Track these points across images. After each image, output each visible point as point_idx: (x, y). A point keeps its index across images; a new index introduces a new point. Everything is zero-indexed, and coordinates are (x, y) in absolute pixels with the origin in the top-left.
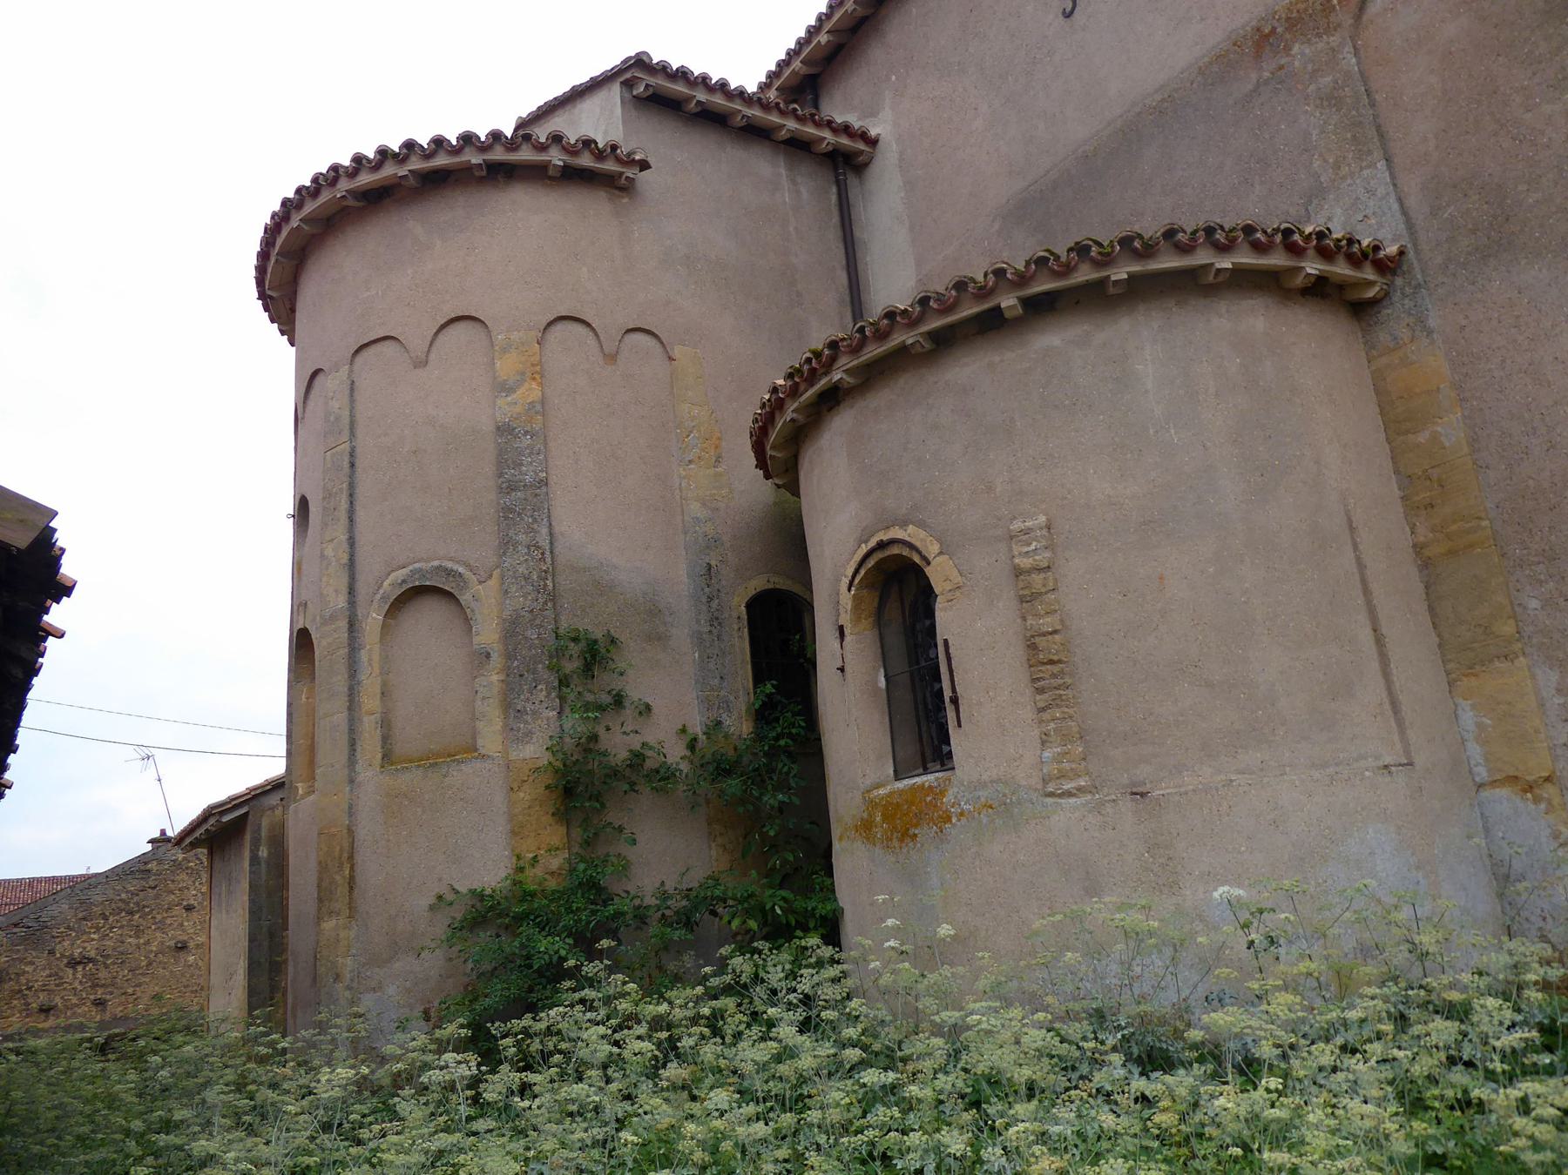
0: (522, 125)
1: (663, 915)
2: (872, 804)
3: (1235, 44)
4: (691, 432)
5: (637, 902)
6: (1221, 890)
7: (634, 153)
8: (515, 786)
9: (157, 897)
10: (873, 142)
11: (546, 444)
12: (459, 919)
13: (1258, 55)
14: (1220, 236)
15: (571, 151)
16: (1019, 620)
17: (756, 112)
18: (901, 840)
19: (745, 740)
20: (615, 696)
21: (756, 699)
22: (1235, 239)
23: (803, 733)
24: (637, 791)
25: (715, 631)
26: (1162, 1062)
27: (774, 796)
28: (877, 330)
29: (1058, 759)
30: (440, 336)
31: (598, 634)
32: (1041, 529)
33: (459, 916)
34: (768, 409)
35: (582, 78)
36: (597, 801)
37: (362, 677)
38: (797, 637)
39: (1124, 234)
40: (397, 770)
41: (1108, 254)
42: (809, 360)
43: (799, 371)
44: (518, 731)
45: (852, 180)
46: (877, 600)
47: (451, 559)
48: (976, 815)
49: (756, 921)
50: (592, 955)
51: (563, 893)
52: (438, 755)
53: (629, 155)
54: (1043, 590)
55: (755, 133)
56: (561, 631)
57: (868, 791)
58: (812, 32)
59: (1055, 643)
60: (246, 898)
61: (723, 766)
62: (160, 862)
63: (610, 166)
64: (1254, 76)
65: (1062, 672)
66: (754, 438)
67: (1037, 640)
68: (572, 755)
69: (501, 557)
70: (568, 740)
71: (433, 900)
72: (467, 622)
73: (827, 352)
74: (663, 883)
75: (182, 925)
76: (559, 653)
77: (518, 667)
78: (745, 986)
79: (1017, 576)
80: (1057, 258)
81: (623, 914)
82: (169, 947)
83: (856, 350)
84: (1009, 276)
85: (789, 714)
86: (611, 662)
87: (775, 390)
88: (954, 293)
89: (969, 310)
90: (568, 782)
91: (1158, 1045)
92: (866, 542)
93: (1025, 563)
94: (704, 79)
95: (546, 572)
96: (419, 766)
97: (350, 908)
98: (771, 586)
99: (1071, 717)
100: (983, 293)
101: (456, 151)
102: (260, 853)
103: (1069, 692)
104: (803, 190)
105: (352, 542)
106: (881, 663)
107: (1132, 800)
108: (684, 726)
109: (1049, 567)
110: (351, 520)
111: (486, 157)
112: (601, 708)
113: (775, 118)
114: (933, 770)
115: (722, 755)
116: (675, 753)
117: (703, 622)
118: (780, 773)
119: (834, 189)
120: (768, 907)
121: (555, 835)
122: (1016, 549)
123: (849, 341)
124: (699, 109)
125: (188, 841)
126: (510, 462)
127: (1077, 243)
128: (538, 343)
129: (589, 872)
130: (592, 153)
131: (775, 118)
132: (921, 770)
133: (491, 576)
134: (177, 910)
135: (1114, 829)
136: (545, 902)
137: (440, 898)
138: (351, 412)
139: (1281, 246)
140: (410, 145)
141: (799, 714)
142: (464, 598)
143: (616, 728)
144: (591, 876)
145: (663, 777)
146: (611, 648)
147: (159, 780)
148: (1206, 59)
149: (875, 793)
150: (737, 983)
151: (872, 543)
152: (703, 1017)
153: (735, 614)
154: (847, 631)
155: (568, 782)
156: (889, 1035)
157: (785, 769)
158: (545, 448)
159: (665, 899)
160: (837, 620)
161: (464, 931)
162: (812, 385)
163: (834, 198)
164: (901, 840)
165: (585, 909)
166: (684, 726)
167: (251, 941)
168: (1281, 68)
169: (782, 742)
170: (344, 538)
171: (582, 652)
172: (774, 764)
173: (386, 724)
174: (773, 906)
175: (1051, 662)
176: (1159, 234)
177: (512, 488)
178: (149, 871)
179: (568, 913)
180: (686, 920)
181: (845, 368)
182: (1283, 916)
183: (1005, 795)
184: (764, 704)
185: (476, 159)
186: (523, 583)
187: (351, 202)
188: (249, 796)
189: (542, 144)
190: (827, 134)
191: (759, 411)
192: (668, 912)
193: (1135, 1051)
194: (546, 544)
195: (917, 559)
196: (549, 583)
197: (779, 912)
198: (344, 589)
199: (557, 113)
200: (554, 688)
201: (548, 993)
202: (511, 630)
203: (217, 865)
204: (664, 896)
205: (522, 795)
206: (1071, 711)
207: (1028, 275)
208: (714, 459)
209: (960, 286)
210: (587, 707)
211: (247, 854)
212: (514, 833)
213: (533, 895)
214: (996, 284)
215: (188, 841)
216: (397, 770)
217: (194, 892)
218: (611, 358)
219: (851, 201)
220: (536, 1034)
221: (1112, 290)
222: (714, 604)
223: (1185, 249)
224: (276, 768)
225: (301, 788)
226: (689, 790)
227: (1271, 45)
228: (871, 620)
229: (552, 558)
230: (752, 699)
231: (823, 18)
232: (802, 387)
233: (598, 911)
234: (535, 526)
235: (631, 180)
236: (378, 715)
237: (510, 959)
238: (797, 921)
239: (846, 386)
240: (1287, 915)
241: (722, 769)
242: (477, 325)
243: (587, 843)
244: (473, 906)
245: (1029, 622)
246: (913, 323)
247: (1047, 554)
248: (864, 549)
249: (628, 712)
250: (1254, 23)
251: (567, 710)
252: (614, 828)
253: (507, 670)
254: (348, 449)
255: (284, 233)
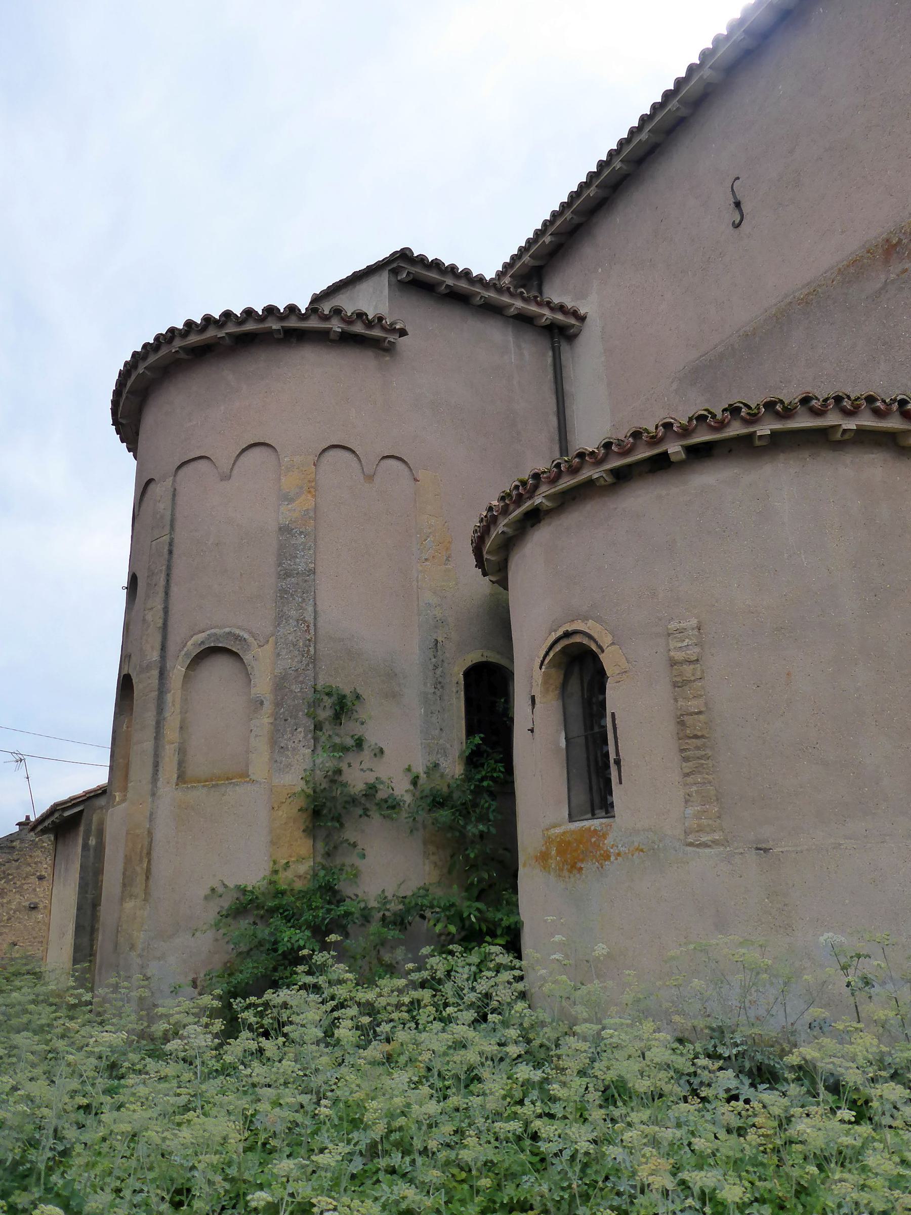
0: (317, 299)
1: (384, 915)
2: (549, 841)
3: (868, 252)
4: (428, 537)
5: (362, 905)
6: (826, 935)
7: (396, 323)
8: (276, 806)
9: (18, 868)
10: (582, 319)
11: (315, 541)
12: (226, 908)
13: (887, 261)
14: (846, 403)
15: (348, 321)
16: (672, 701)
17: (491, 294)
18: (570, 871)
19: (457, 779)
20: (357, 740)
21: (467, 747)
22: (859, 406)
23: (502, 776)
24: (368, 816)
25: (438, 693)
26: (769, 1077)
27: (476, 826)
28: (570, 466)
29: (698, 816)
30: (242, 457)
31: (347, 691)
32: (693, 629)
33: (226, 905)
34: (485, 523)
35: (345, 273)
36: (338, 821)
37: (167, 714)
38: (503, 700)
39: (769, 399)
40: (188, 788)
41: (755, 415)
42: (517, 487)
43: (509, 495)
44: (281, 763)
45: (565, 347)
46: (562, 677)
47: (238, 628)
48: (630, 856)
49: (455, 926)
50: (325, 947)
51: (306, 893)
52: (219, 778)
53: (391, 324)
54: (693, 678)
55: (491, 310)
56: (319, 687)
57: (547, 830)
58: (538, 234)
59: (700, 721)
60: (78, 875)
61: (438, 799)
62: (22, 841)
63: (377, 333)
64: (883, 277)
65: (704, 745)
66: (474, 545)
67: (686, 718)
68: (321, 784)
69: (276, 627)
70: (318, 772)
71: (208, 892)
72: (248, 676)
73: (531, 481)
74: (383, 891)
75: (34, 890)
76: (316, 703)
77: (284, 713)
78: (440, 982)
79: (672, 666)
80: (714, 416)
81: (351, 914)
82: (24, 907)
83: (553, 481)
84: (675, 428)
85: (492, 762)
86: (355, 713)
87: (490, 509)
88: (631, 440)
89: (643, 453)
90: (315, 806)
91: (766, 1062)
92: (555, 631)
93: (679, 656)
94: (453, 268)
95: (309, 640)
96: (204, 786)
97: (145, 894)
98: (484, 659)
99: (710, 782)
100: (655, 441)
101: (261, 319)
102: (90, 842)
103: (710, 762)
104: (526, 353)
105: (166, 610)
106: (563, 727)
107: (757, 854)
108: (410, 766)
109: (697, 660)
110: (167, 593)
111: (283, 325)
112: (345, 749)
113: (506, 299)
114: (600, 816)
115: (438, 791)
116: (401, 789)
117: (429, 685)
118: (483, 806)
119: (550, 353)
120: (465, 915)
121: (304, 846)
122: (673, 644)
123: (548, 474)
124: (448, 291)
125: (40, 828)
126: (287, 555)
127: (730, 405)
128: (315, 465)
129: (327, 878)
130: (363, 322)
131: (506, 299)
132: (589, 816)
133: (268, 641)
134: (33, 879)
135: (741, 877)
136: (293, 899)
137: (213, 890)
138: (172, 511)
139: (897, 413)
140: (227, 314)
141: (500, 761)
142: (247, 657)
143: (356, 765)
144: (329, 881)
145: (391, 806)
146: (355, 703)
147: (28, 778)
148: (845, 263)
149: (552, 831)
150: (433, 978)
151: (560, 633)
152: (403, 1004)
153: (454, 680)
154: (537, 700)
155: (315, 806)
156: (546, 1035)
157: (486, 805)
158: (315, 544)
159: (385, 904)
160: (530, 691)
161: (229, 919)
162: (519, 506)
163: (550, 360)
164: (570, 871)
165: (322, 908)
166: (410, 766)
167: (78, 909)
168: (906, 271)
169: (485, 784)
170: (160, 607)
171: (334, 704)
172: (478, 800)
173: (182, 751)
174: (470, 914)
175: (696, 737)
176: (797, 400)
177: (287, 575)
178: (14, 847)
179: (309, 910)
180: (400, 922)
181: (544, 495)
182: (875, 963)
183: (653, 842)
184: (473, 753)
185: (276, 326)
186: (291, 648)
187: (183, 355)
188: (70, 804)
189: (326, 315)
190: (546, 312)
191: (479, 525)
192: (387, 914)
193: (747, 1065)
194: (310, 618)
195: (594, 647)
196: (312, 649)
197: (473, 919)
198: (158, 646)
199: (342, 292)
200: (310, 731)
201: (287, 973)
202: (280, 685)
203: (60, 847)
204: (385, 901)
205: (280, 813)
206: (710, 777)
207: (690, 428)
208: (445, 558)
209: (636, 435)
210: (335, 748)
211: (80, 841)
212: (272, 843)
213: (283, 893)
214: (665, 434)
215: (40, 828)
216: (188, 788)
217: (45, 866)
218: (370, 478)
219: (564, 362)
220: (274, 1007)
221: (757, 443)
222: (439, 671)
223: (818, 413)
224: (99, 777)
225: (118, 796)
226: (410, 817)
227: (898, 253)
228: (557, 692)
229: (315, 630)
230: (464, 747)
231: (548, 224)
232: (511, 508)
233: (331, 910)
234: (304, 605)
235: (392, 344)
236: (176, 745)
237: (261, 944)
238: (488, 928)
239: (545, 508)
240: (879, 962)
241: (437, 802)
242: (269, 450)
243: (328, 855)
244: (237, 899)
245: (680, 703)
246: (599, 462)
247: (697, 650)
248: (554, 636)
249: (367, 753)
250: (884, 236)
251: (319, 749)
252: (349, 844)
253: (275, 716)
254: (168, 540)
255: (133, 377)
